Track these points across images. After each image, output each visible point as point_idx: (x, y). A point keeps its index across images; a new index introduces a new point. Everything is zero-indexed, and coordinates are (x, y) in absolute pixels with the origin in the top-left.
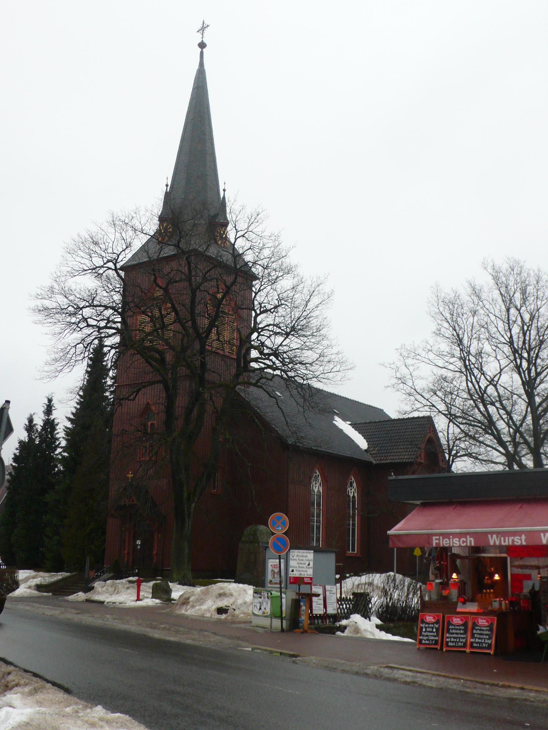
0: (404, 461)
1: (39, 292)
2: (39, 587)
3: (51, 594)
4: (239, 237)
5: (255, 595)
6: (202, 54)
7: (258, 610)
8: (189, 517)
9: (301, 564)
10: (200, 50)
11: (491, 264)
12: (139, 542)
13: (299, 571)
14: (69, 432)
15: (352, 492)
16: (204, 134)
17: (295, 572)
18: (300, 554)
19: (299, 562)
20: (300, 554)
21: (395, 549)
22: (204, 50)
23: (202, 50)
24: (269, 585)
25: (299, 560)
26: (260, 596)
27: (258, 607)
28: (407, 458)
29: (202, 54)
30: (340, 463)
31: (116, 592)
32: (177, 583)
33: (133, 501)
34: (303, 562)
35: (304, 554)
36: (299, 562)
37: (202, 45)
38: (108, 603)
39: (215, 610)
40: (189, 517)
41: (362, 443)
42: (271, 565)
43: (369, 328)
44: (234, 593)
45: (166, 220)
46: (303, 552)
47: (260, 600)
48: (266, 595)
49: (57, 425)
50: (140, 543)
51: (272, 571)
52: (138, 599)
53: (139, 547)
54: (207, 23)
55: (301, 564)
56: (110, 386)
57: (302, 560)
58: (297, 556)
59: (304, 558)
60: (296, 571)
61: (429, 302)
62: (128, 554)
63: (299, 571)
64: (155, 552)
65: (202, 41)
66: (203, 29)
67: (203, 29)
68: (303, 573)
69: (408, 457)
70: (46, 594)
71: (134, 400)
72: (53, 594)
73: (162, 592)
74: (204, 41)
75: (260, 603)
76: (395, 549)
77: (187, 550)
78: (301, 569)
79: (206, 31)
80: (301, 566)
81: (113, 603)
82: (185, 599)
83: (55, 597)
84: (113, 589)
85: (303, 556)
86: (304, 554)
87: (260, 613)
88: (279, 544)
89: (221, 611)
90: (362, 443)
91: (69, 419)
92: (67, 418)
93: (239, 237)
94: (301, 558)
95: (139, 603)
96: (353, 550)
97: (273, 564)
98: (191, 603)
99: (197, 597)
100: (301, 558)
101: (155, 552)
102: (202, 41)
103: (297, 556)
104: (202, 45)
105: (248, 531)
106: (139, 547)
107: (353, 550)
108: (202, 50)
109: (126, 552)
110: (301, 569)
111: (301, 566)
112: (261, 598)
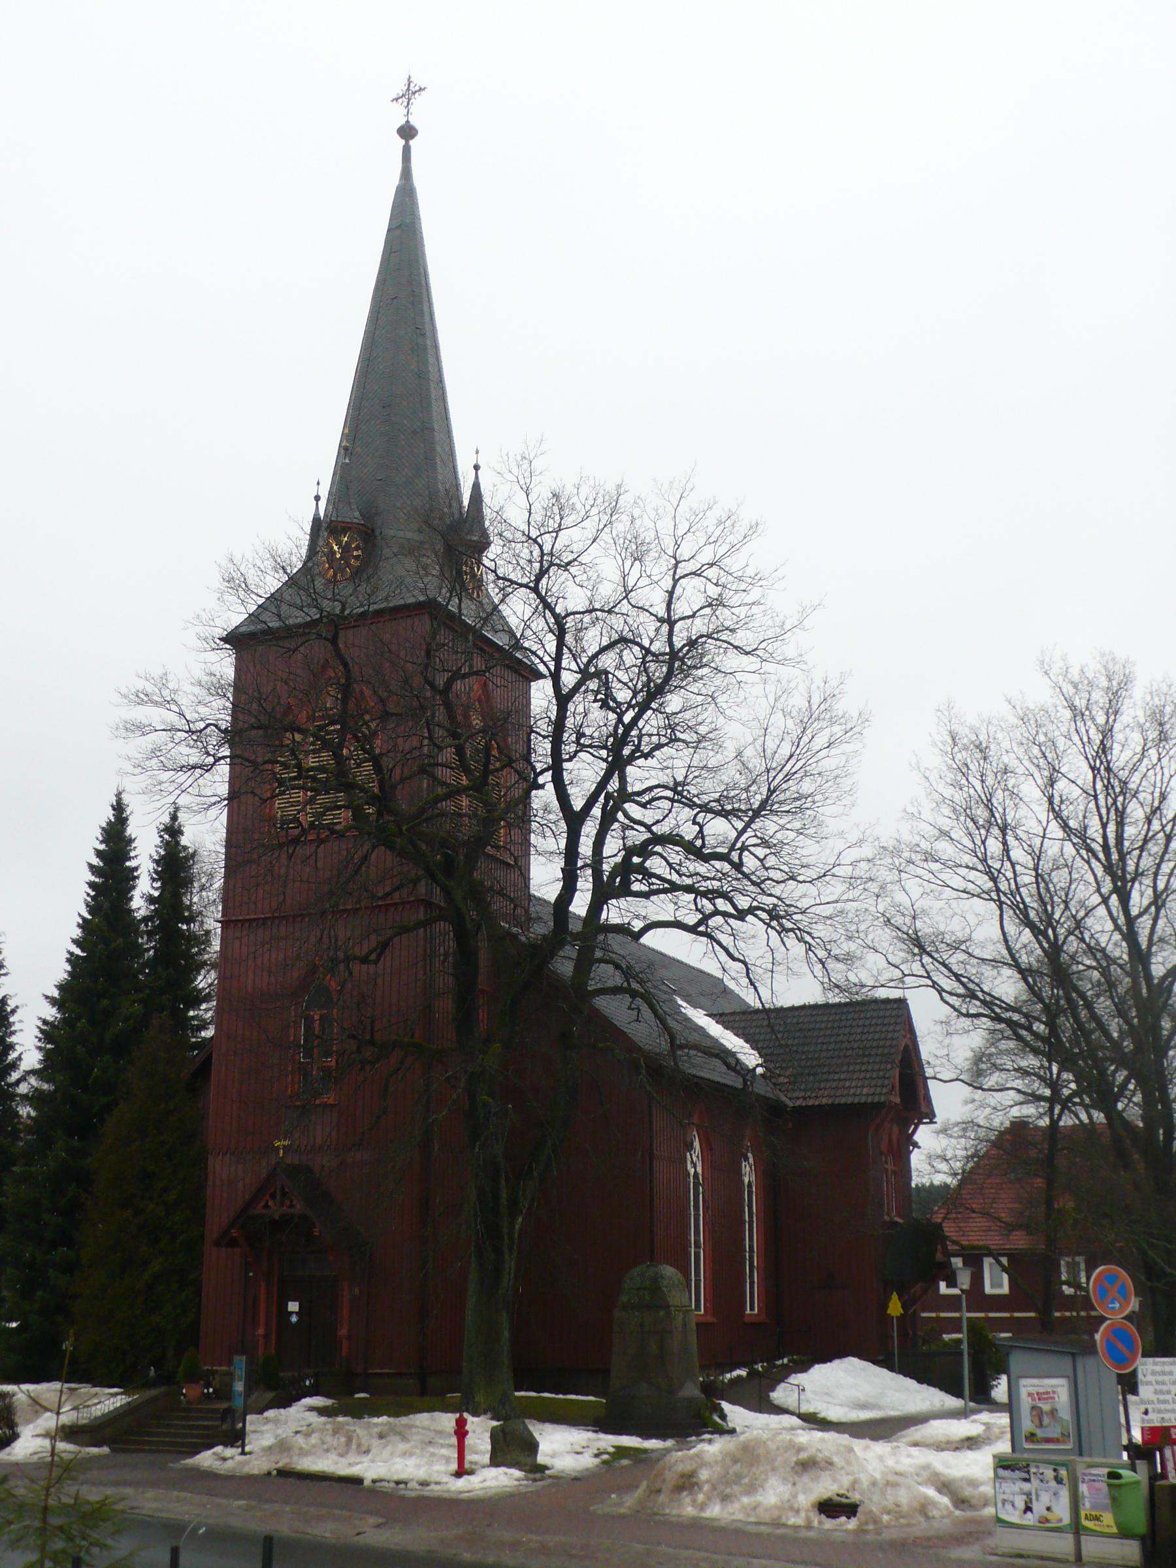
0: (863, 1100)
1: (140, 684)
2: (71, 1433)
3: (105, 1450)
4: (681, 578)
5: (1001, 1472)
6: (407, 152)
7: (1017, 1513)
8: (511, 1249)
9: (1161, 1392)
10: (403, 142)
11: (1061, 664)
12: (293, 1306)
13: (1159, 1411)
14: (49, 1032)
15: (748, 1173)
16: (424, 335)
17: (1151, 1416)
18: (1158, 1368)
19: (1159, 1387)
20: (1158, 1368)
21: (957, 1315)
22: (411, 142)
23: (407, 142)
24: (1027, 1446)
25: (1157, 1383)
26: (1025, 1476)
27: (1022, 1506)
28: (868, 1095)
29: (407, 152)
30: (723, 1104)
31: (354, 1447)
32: (489, 1415)
33: (291, 1206)
34: (1165, 1388)
35: (1167, 1368)
36: (1159, 1387)
37: (407, 132)
38: (374, 1481)
39: (813, 1506)
40: (511, 1249)
41: (750, 1058)
42: (1030, 1395)
43: (851, 799)
44: (835, 1459)
45: (350, 528)
46: (1164, 1363)
47: (1026, 1486)
48: (1049, 1473)
49: (13, 1011)
50: (297, 1309)
51: (1033, 1408)
52: (460, 1473)
53: (294, 1319)
54: (418, 82)
55: (1161, 1392)
56: (146, 919)
57: (1163, 1383)
58: (1154, 1373)
59: (1166, 1378)
60: (1154, 1411)
61: (934, 744)
62: (266, 1337)
63: (1159, 1411)
64: (344, 1332)
65: (408, 122)
66: (409, 94)
67: (409, 94)
68: (1167, 1416)
69: (872, 1091)
70: (94, 1450)
71: (376, 962)
72: (113, 1450)
73: (513, 1448)
74: (413, 122)
75: (1028, 1494)
76: (957, 1315)
77: (506, 1334)
78: (1162, 1407)
79: (417, 101)
80: (1162, 1397)
81: (398, 1483)
82: (682, 1476)
83: (122, 1458)
84: (343, 1439)
85: (1164, 1373)
86: (1167, 1368)
87: (1030, 1519)
88: (1120, 1346)
89: (830, 1508)
90: (750, 1058)
91: (53, 1001)
92: (47, 997)
93: (681, 578)
94: (1160, 1378)
95: (462, 1484)
96: (752, 1309)
97: (1033, 1390)
98: (706, 1488)
99: (718, 1469)
100: (1160, 1378)
101: (344, 1332)
102: (408, 122)
103: (1154, 1373)
104: (407, 132)
105: (636, 1276)
106: (294, 1319)
107: (752, 1309)
108: (407, 142)
109: (261, 1331)
110: (1162, 1407)
111: (1162, 1397)
112: (1027, 1480)
